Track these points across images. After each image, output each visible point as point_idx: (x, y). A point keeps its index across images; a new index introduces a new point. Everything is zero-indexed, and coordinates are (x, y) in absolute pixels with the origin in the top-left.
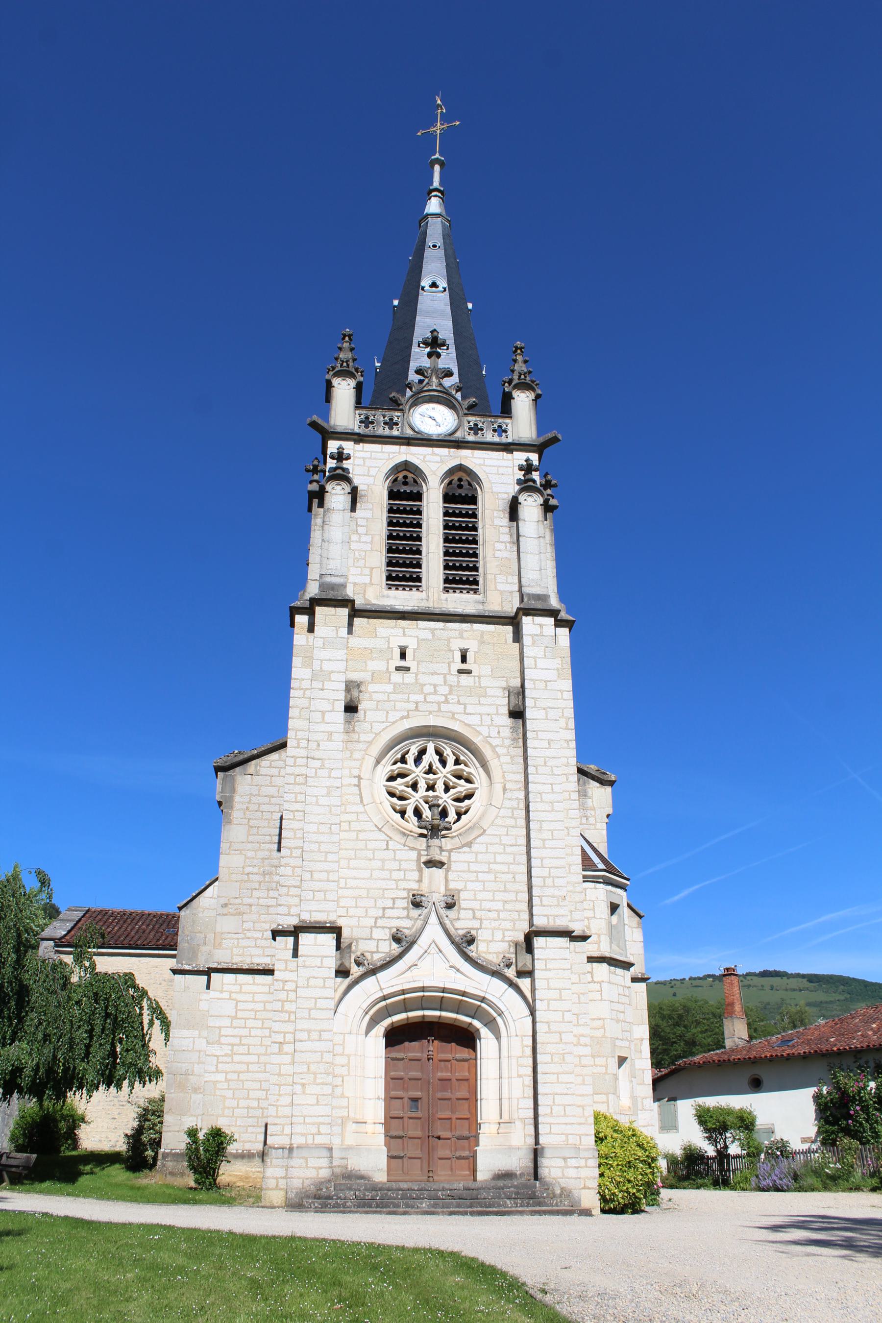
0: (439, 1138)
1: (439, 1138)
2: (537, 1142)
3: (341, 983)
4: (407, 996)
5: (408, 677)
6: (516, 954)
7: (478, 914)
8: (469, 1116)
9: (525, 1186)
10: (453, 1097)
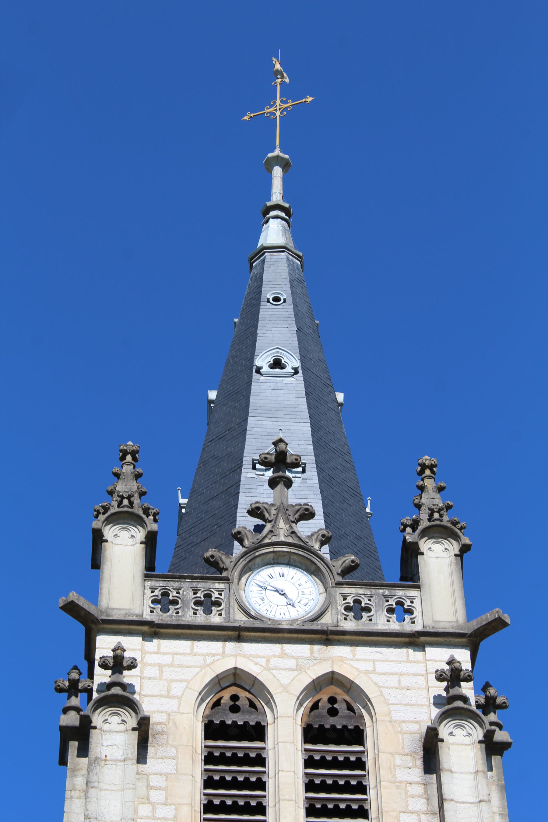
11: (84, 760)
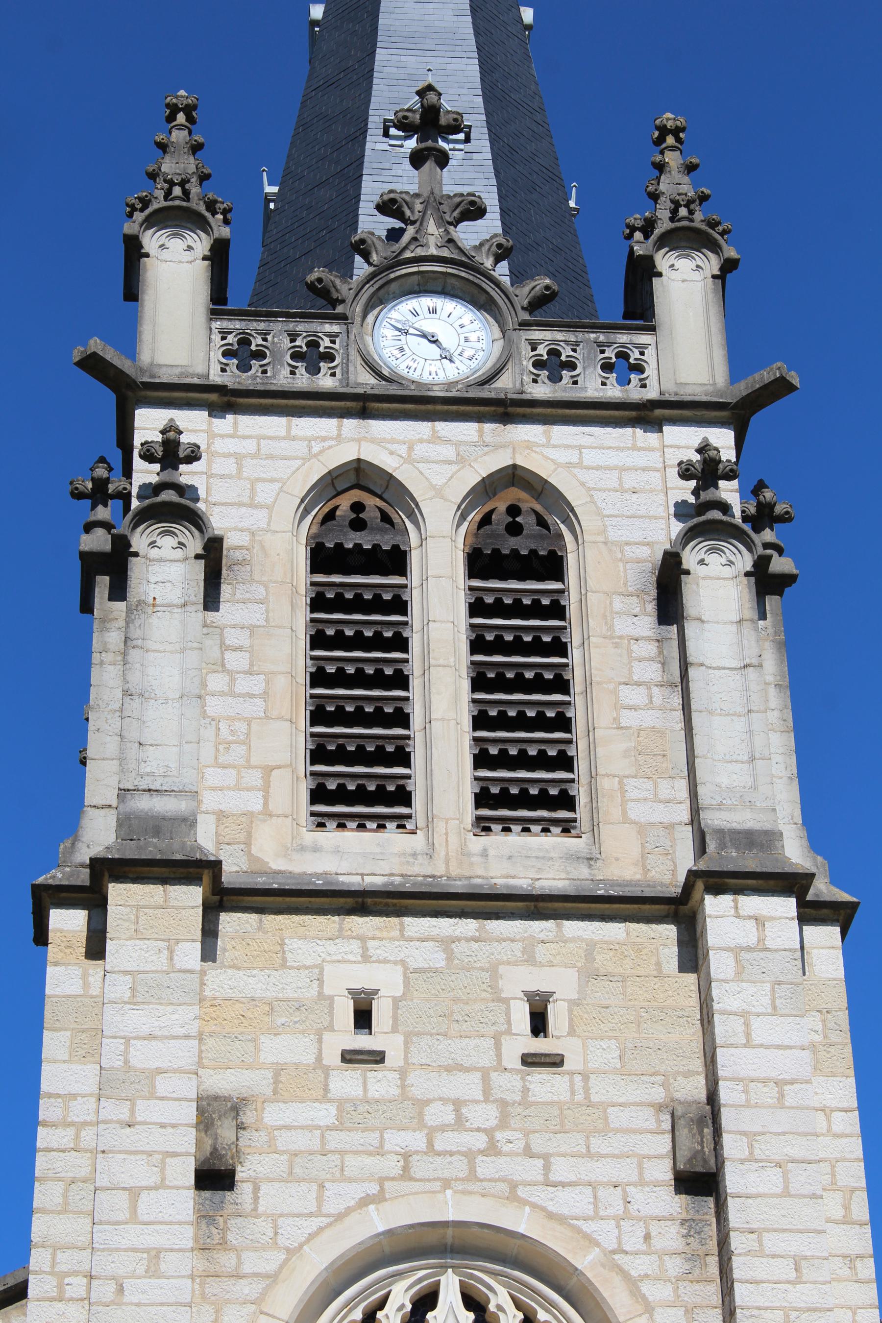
5: (380, 1083)
11: (121, 606)
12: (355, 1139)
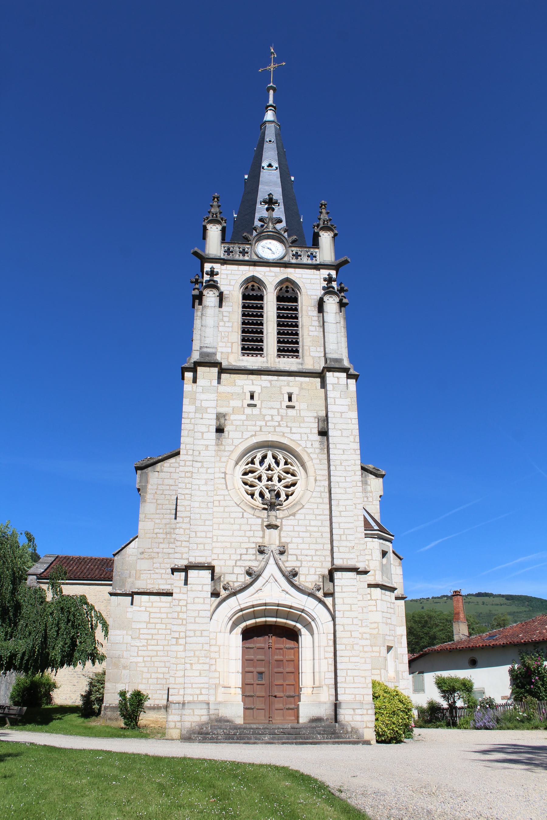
0: (275, 697)
1: (275, 697)
2: (336, 699)
3: (215, 601)
4: (255, 609)
5: (255, 411)
6: (323, 582)
7: (300, 558)
8: (294, 683)
9: (329, 726)
10: (285, 671)
12: (250, 423)
